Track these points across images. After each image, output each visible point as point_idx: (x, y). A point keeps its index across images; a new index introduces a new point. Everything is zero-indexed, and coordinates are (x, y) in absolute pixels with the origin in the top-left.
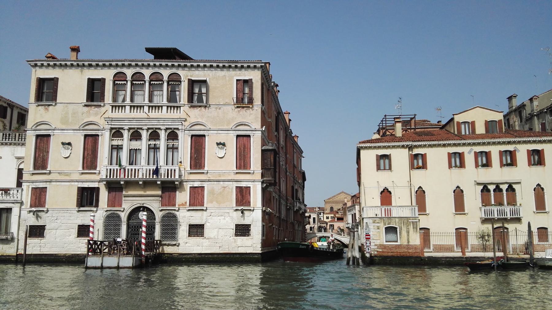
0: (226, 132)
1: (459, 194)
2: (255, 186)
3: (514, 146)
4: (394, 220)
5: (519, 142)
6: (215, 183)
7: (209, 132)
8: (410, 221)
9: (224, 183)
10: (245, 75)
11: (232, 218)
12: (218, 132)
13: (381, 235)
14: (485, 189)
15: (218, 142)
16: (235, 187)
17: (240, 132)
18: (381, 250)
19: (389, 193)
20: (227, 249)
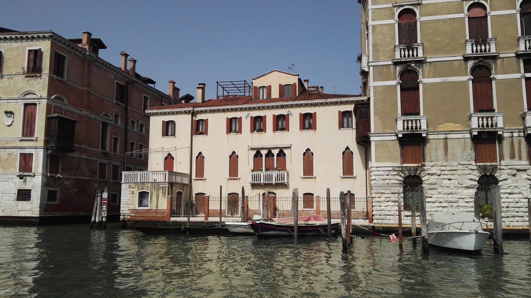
0: (16, 101)
1: (234, 158)
2: (37, 153)
3: (288, 110)
4: (146, 185)
5: (292, 106)
6: (2, 150)
7: (40, 100)
8: (160, 186)
9: (10, 150)
10: (36, 45)
11: (15, 183)
12: (9, 101)
13: (135, 200)
14: (258, 155)
15: (8, 110)
16: (19, 154)
17: (27, 101)
18: (133, 215)
19: (172, 159)
20: (9, 213)
